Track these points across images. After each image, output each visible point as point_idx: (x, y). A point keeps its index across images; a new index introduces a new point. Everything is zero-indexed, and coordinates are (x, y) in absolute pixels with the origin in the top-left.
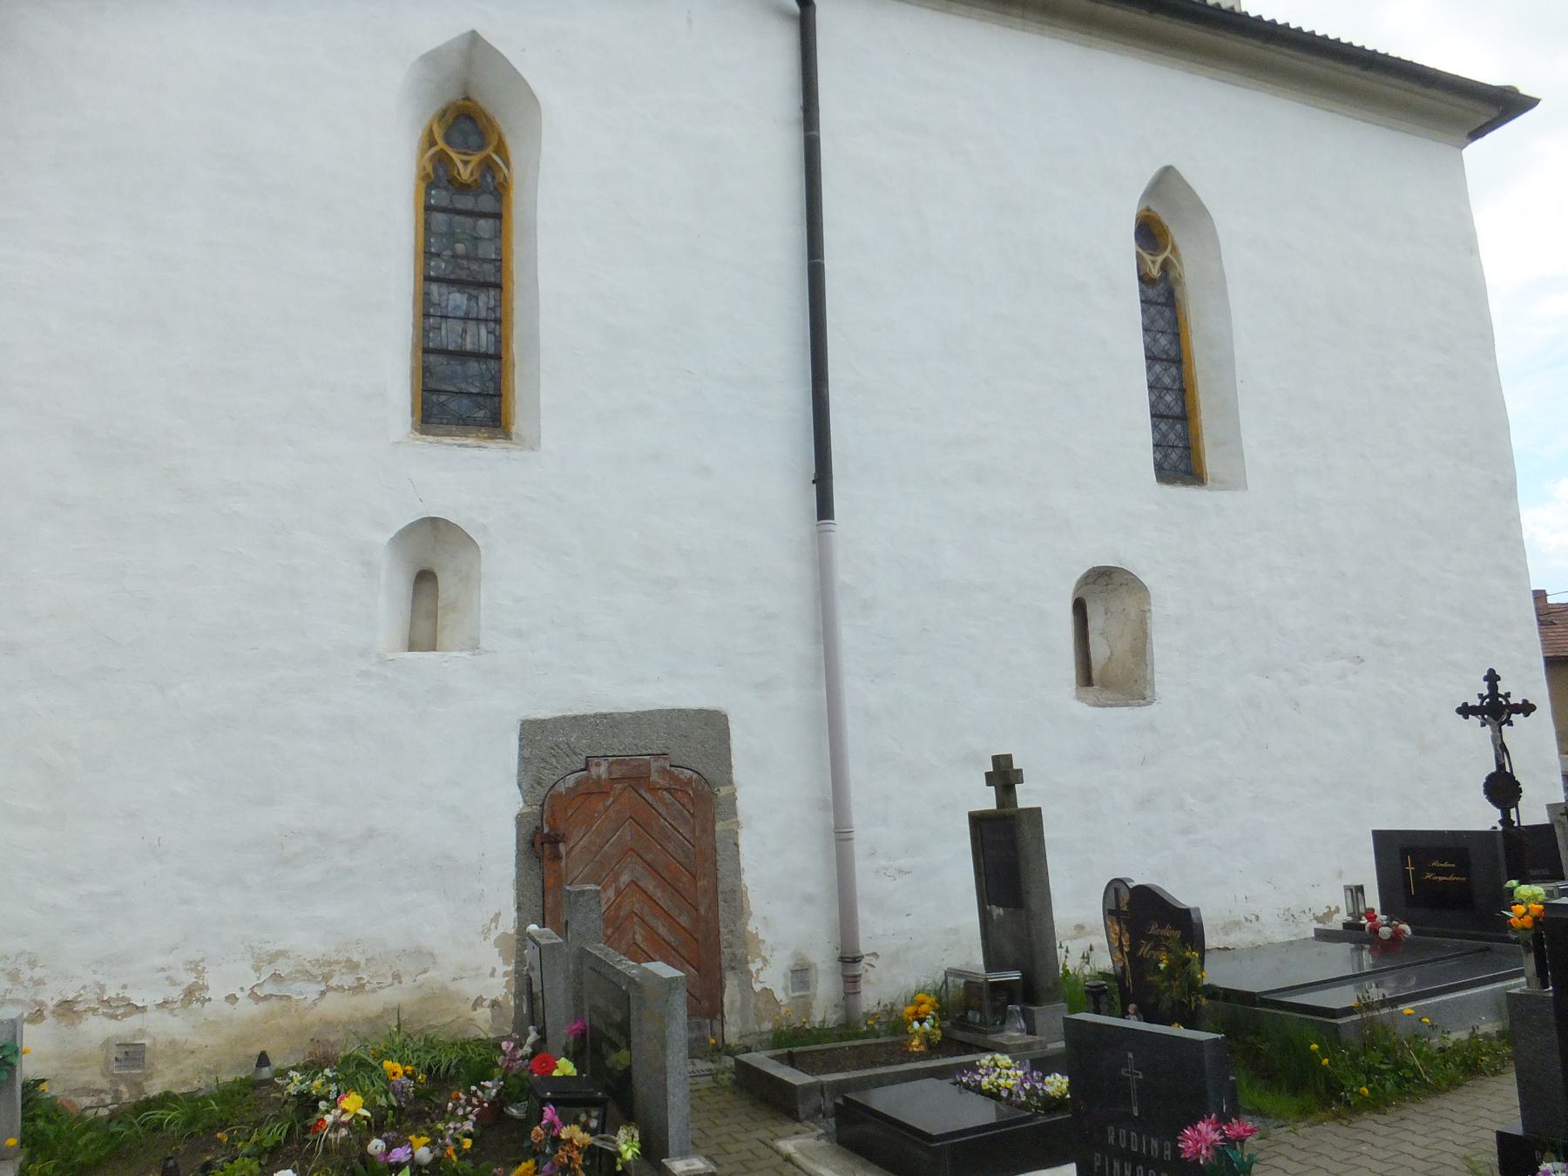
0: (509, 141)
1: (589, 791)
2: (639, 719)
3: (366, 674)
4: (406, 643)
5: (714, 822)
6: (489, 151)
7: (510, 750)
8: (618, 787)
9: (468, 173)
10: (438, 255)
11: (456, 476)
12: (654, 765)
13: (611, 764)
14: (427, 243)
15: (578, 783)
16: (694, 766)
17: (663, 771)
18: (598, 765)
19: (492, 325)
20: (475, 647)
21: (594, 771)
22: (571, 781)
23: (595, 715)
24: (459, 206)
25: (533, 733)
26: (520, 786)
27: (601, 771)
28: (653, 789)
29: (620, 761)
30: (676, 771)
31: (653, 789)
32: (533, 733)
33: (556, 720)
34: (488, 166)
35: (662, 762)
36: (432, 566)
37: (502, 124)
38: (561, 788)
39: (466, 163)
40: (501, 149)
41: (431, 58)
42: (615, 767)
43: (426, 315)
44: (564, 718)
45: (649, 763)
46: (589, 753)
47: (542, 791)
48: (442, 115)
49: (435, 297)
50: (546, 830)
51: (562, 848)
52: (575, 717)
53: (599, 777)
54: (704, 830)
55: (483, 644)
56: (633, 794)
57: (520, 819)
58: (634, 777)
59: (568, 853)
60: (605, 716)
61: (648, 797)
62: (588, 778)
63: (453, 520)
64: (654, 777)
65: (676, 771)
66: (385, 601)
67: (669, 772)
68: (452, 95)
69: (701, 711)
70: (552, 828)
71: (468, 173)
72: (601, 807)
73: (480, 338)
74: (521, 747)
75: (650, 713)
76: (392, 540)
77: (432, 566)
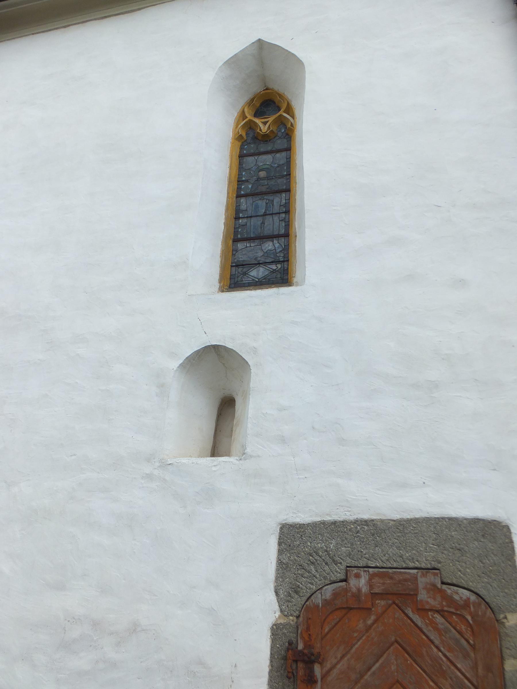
0: (294, 104)
1: (345, 606)
2: (406, 529)
3: (149, 477)
4: (209, 447)
5: (502, 659)
6: (281, 112)
7: (267, 555)
8: (381, 603)
9: (266, 131)
10: (247, 181)
11: (246, 319)
12: (422, 581)
13: (372, 577)
14: (240, 175)
15: (336, 595)
16: (471, 585)
17: (433, 589)
18: (358, 576)
19: (283, 215)
20: (243, 455)
21: (353, 582)
22: (328, 592)
23: (356, 522)
24: (262, 150)
25: (293, 538)
26: (277, 593)
27: (361, 583)
28: (422, 611)
29: (381, 573)
30: (449, 590)
31: (422, 611)
32: (293, 538)
33: (314, 525)
34: (281, 122)
35: (431, 578)
36: (220, 383)
37: (288, 95)
38: (318, 599)
39: (265, 123)
40: (289, 110)
41: (233, 62)
42: (376, 580)
43: (237, 218)
44: (323, 523)
45: (415, 578)
46: (349, 561)
47: (298, 601)
48: (251, 102)
49: (243, 207)
50: (301, 647)
51: (317, 670)
52: (334, 523)
53: (359, 590)
54: (488, 669)
55: (248, 450)
56: (399, 614)
57: (276, 630)
58: (397, 592)
59: (323, 677)
60: (366, 522)
61: (417, 618)
62: (346, 590)
63: (229, 345)
64: (423, 595)
65: (449, 590)
66: (185, 415)
67: (441, 591)
68: (256, 88)
69: (476, 521)
70: (307, 645)
71: (266, 131)
72: (361, 625)
73: (273, 225)
74: (280, 552)
75: (416, 521)
76: (181, 365)
77: (220, 383)
